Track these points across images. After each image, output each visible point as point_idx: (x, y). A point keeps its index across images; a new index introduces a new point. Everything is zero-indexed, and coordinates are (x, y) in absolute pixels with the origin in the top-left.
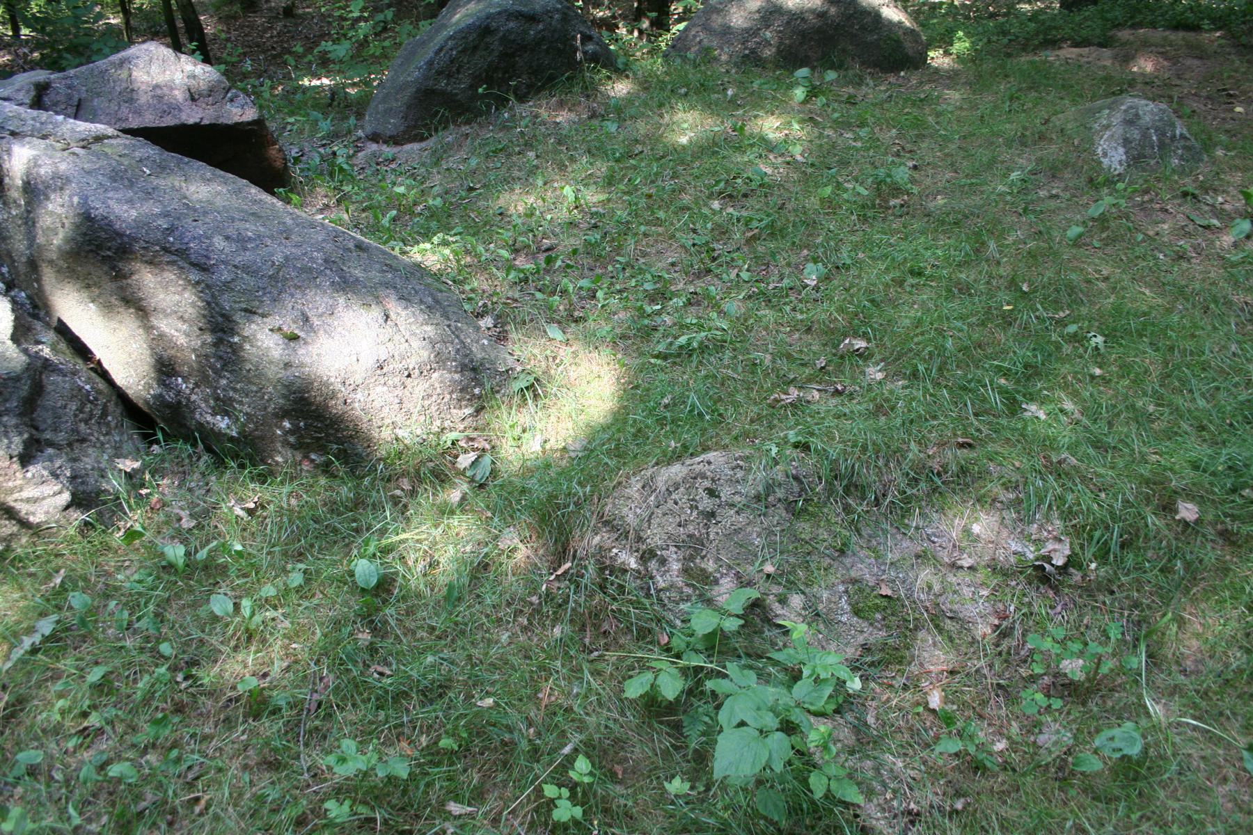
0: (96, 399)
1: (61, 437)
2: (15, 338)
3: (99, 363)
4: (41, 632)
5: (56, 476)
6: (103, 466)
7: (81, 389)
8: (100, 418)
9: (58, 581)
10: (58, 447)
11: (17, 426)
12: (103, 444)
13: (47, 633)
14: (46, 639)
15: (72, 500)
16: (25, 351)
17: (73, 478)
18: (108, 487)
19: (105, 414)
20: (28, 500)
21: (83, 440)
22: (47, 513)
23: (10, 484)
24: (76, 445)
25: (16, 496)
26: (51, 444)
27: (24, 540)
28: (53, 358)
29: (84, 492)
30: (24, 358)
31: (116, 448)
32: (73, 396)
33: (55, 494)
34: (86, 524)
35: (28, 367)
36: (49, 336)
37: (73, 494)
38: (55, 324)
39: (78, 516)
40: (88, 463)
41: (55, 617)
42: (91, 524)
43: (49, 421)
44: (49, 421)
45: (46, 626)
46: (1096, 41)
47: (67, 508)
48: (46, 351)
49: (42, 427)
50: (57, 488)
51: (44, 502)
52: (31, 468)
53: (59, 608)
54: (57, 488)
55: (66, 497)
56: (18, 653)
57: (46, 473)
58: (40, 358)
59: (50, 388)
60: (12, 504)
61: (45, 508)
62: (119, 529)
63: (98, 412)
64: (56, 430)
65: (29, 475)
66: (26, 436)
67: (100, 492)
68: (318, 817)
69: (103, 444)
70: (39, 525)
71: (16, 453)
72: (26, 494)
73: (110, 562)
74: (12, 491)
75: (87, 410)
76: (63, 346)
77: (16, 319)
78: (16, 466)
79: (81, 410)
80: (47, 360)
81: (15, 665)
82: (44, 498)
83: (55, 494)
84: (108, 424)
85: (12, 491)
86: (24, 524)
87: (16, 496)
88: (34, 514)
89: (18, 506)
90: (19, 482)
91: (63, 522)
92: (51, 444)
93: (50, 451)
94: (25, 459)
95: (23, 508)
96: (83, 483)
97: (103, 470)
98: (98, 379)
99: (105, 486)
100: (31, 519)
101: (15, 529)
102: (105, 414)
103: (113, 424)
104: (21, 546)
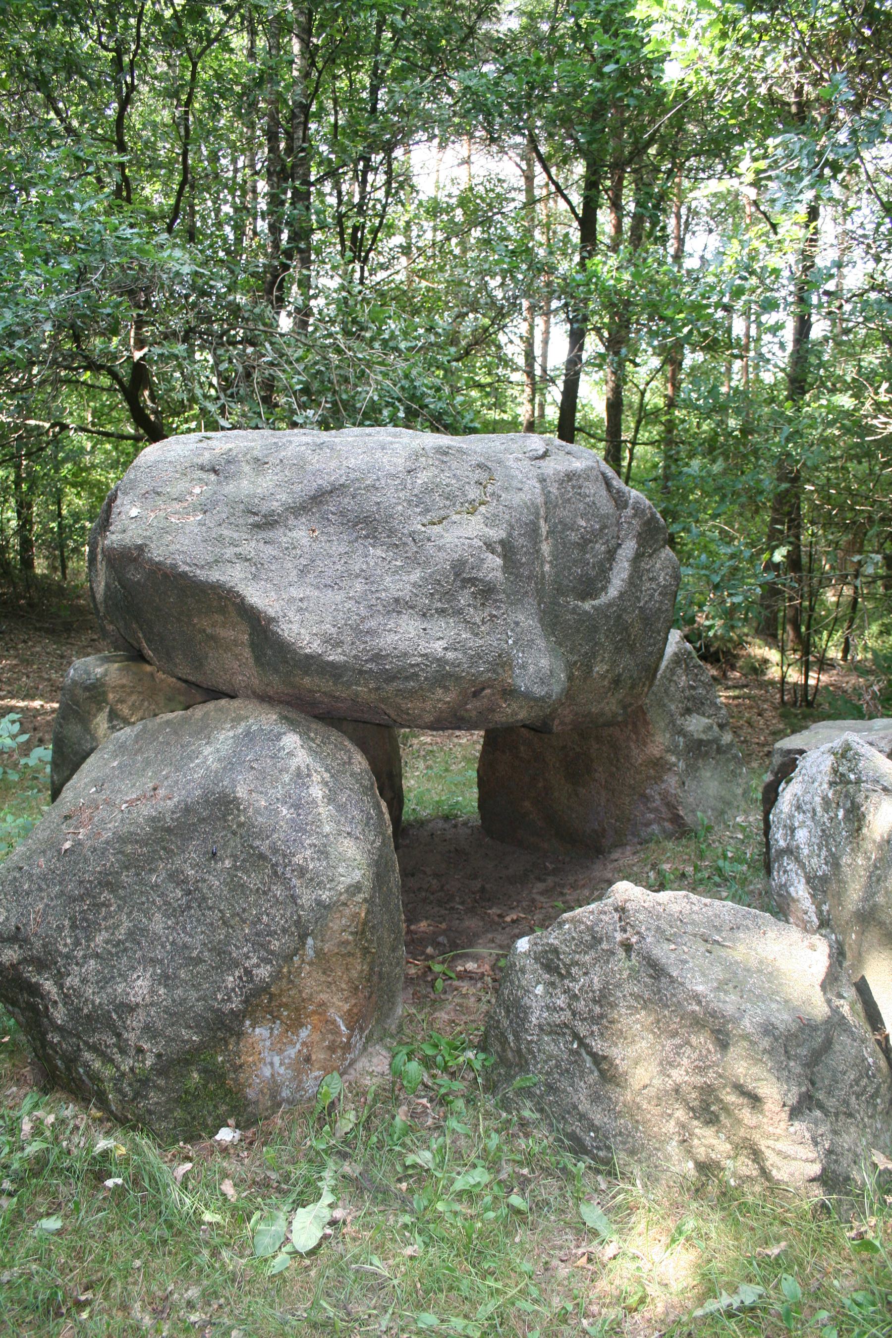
0: (874, 1076)
1: (831, 1103)
2: (823, 986)
3: (887, 1038)
4: (743, 1297)
5: (816, 1144)
6: (859, 1150)
7: (864, 1059)
8: (872, 1097)
9: (776, 1251)
10: (826, 1113)
11: (799, 1076)
12: (865, 1126)
13: (747, 1303)
14: (742, 1309)
15: (821, 1176)
16: (829, 1001)
17: (830, 1152)
18: (857, 1178)
19: (874, 1096)
20: (779, 1153)
21: (850, 1115)
22: (792, 1175)
23: (771, 1129)
24: (842, 1117)
25: (770, 1143)
26: (821, 1106)
27: (757, 1189)
28: (849, 1018)
29: (834, 1172)
30: (827, 1009)
31: (875, 1136)
32: (855, 1065)
33: (807, 1160)
34: (823, 1205)
35: (828, 1021)
36: (850, 993)
37: (824, 1170)
38: (856, 979)
39: (818, 1193)
40: (846, 1141)
41: (759, 1289)
42: (827, 1208)
43: (826, 1082)
44: (826, 1082)
45: (749, 1294)
46: (428, 718)
47: (813, 1180)
48: (846, 1010)
49: (819, 1085)
50: (812, 1155)
51: (793, 1162)
52: (796, 1123)
53: (765, 1281)
54: (812, 1155)
55: (815, 1169)
56: (711, 1305)
57: (808, 1135)
58: (839, 1013)
59: (837, 1047)
60: (763, 1149)
61: (792, 1169)
62: (852, 1228)
63: (870, 1090)
64: (829, 1093)
65: (792, 1129)
66: (804, 1089)
67: (848, 1179)
68: (116, 358)
69: (865, 1126)
70: (778, 1182)
71: (789, 1103)
72: (779, 1146)
73: (831, 1260)
74: (768, 1136)
75: (863, 1083)
76: (859, 1007)
77: (830, 966)
78: (785, 1116)
79: (857, 1082)
80: (843, 1017)
81: (705, 1316)
82: (795, 1159)
83: (807, 1160)
84: (875, 1106)
85: (768, 1136)
86: (765, 1173)
87: (770, 1143)
88: (779, 1169)
89: (768, 1153)
90: (778, 1131)
91: (802, 1191)
92: (821, 1106)
93: (818, 1113)
94: (795, 1113)
95: (771, 1159)
96: (836, 1161)
97: (856, 1155)
98: (881, 1056)
99: (854, 1174)
100: (774, 1172)
101: (755, 1173)
102: (874, 1096)
103: (880, 1108)
104: (753, 1194)
